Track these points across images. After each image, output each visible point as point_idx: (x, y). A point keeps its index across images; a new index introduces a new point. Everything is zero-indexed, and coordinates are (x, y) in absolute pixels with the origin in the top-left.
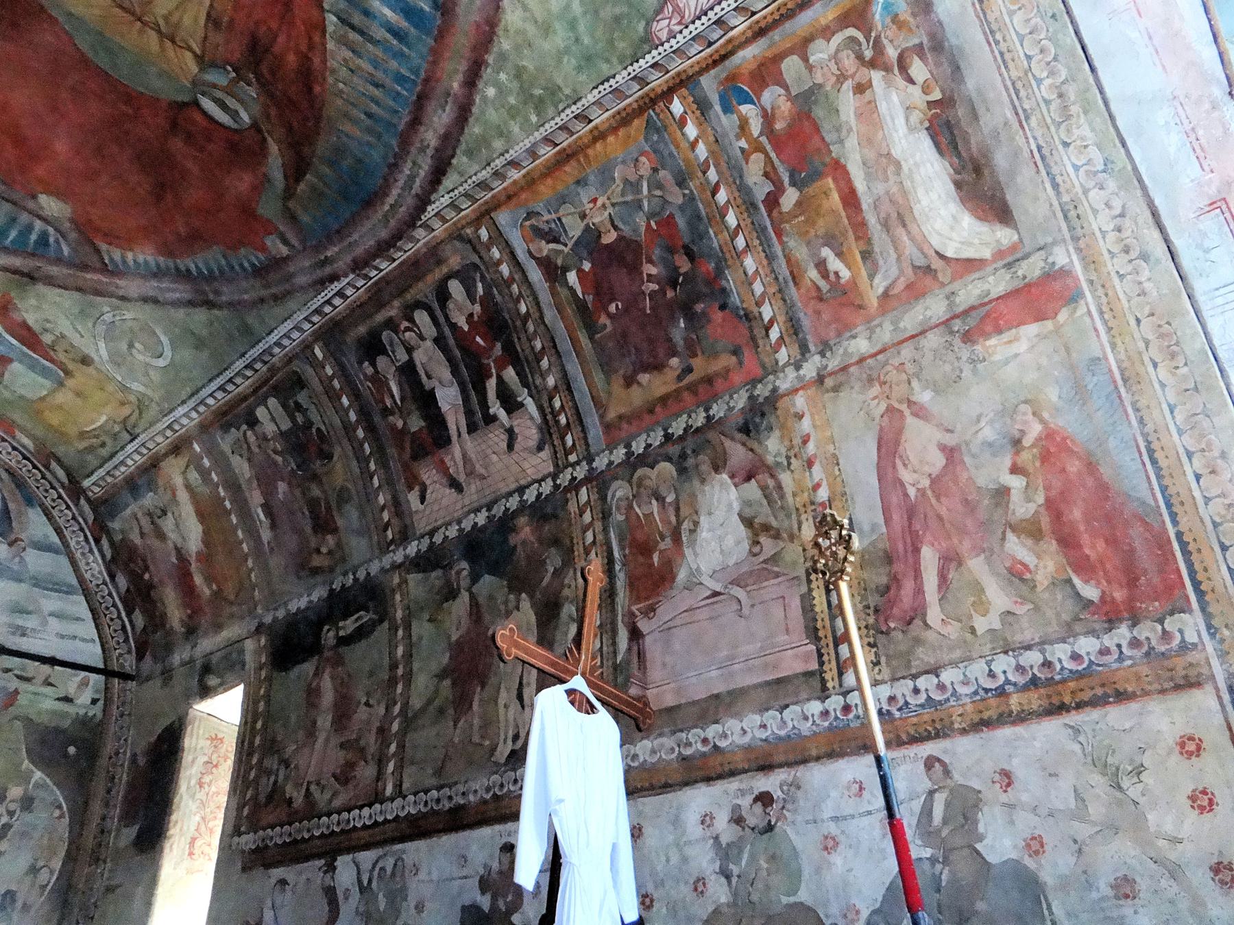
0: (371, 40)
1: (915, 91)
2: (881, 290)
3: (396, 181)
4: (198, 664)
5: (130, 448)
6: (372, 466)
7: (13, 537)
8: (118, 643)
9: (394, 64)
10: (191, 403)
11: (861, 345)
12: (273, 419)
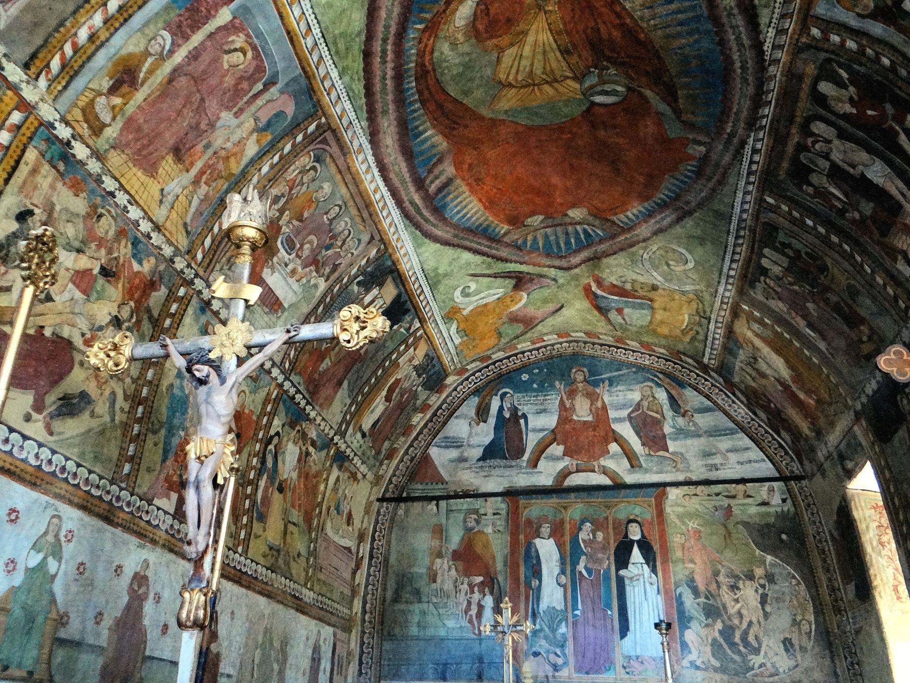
3: (731, 50)
4: (835, 455)
5: (712, 326)
6: (859, 259)
7: (682, 411)
8: (782, 457)
10: (723, 281)
12: (776, 263)
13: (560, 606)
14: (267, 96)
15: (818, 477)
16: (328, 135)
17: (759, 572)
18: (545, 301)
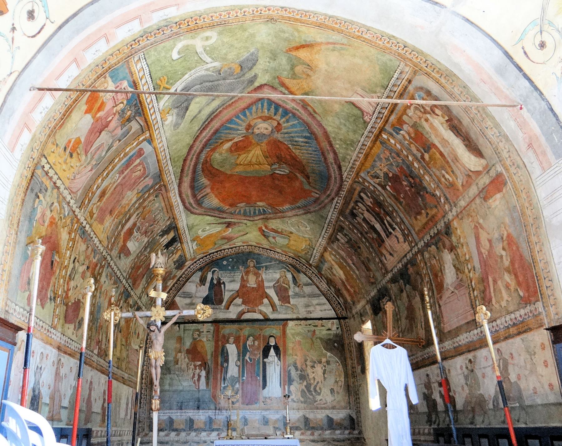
0: (301, 146)
1: (441, 118)
2: (461, 184)
5: (315, 251)
9: (310, 149)
10: (321, 238)
11: (462, 203)
13: (237, 376)
14: (144, 181)
15: (352, 319)
16: (163, 188)
17: (324, 360)
18: (240, 231)
